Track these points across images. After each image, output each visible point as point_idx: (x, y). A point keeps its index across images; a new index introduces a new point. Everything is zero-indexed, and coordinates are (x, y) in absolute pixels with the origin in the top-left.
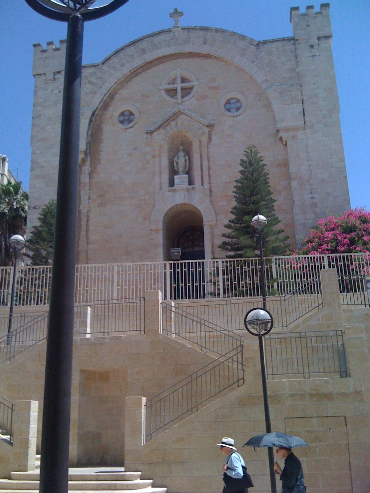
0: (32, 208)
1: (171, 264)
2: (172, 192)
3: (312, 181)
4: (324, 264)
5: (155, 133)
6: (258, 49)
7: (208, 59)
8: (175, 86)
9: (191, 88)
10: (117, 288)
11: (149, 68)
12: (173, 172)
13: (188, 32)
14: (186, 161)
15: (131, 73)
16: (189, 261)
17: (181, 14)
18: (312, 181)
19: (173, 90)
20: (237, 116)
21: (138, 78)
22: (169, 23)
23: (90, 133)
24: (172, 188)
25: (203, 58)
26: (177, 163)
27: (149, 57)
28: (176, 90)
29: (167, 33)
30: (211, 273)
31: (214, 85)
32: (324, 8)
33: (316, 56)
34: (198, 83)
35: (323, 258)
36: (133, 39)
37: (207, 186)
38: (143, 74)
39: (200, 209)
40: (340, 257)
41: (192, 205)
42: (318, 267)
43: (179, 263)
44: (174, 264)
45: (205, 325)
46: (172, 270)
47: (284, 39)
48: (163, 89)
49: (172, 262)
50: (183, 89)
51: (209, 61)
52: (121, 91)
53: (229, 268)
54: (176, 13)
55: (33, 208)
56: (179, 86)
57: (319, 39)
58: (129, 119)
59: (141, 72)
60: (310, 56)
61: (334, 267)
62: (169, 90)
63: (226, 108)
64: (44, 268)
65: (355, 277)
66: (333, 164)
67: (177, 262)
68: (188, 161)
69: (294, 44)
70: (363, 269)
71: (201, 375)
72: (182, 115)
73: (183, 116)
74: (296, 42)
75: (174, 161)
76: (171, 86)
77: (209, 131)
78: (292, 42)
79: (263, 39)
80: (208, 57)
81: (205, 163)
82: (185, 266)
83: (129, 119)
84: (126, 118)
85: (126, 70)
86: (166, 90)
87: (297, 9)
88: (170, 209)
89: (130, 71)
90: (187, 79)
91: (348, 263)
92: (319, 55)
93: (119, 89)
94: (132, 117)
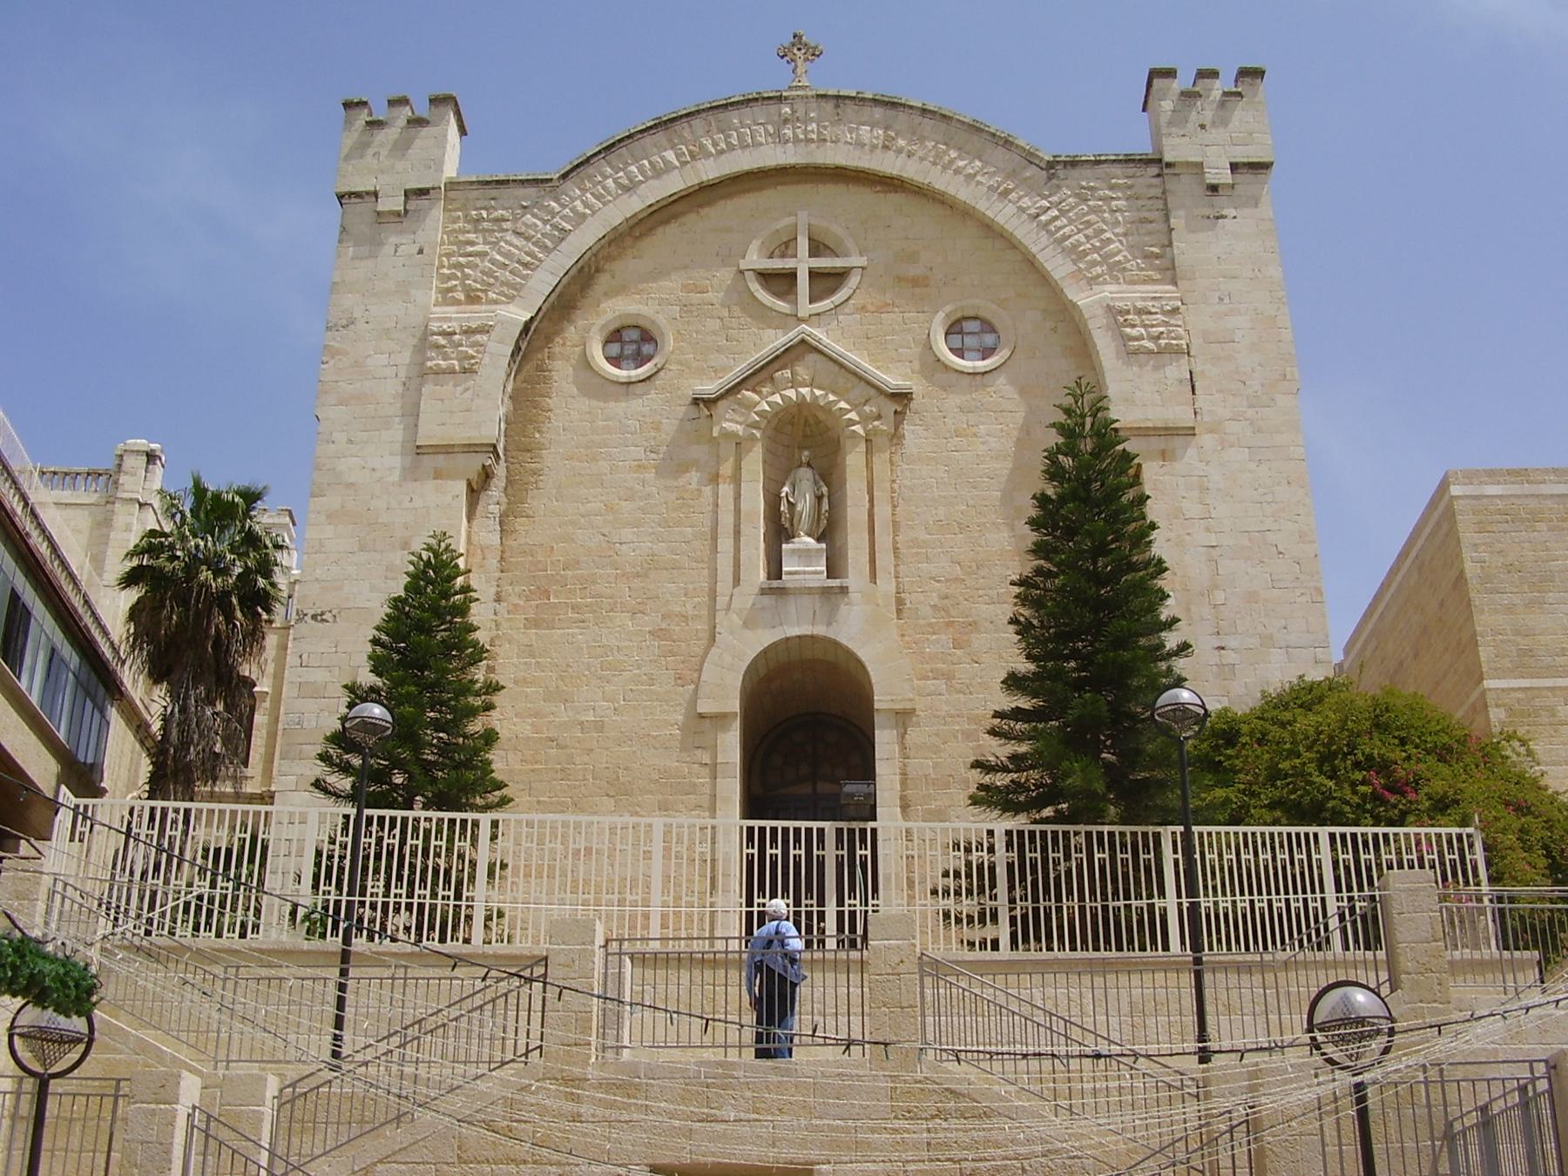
0: (308, 619)
1: (839, 831)
2: (774, 597)
3: (1220, 597)
4: (1176, 856)
5: (721, 404)
6: (1050, 179)
7: (896, 192)
8: (789, 264)
9: (839, 274)
10: (838, 912)
11: (709, 203)
12: (779, 531)
13: (837, 106)
14: (819, 498)
15: (651, 213)
16: (797, 824)
17: (814, 53)
18: (1220, 597)
19: (783, 274)
20: (986, 372)
21: (672, 230)
22: (774, 78)
23: (509, 389)
24: (775, 584)
25: (879, 188)
26: (791, 505)
27: (709, 170)
28: (791, 276)
29: (771, 102)
30: (960, 873)
31: (914, 271)
32: (1247, 80)
33: (1223, 217)
34: (862, 261)
35: (1316, 835)
36: (666, 112)
37: (886, 585)
38: (691, 217)
39: (862, 654)
40: (1449, 836)
41: (836, 644)
42: (1369, 869)
43: (866, 829)
44: (851, 831)
45: (1462, 1117)
46: (845, 853)
47: (1129, 160)
48: (753, 270)
49: (844, 825)
50: (814, 274)
51: (896, 198)
52: (617, 266)
53: (1061, 855)
54: (798, 48)
55: (314, 617)
56: (803, 263)
57: (1234, 167)
58: (638, 352)
59: (683, 214)
60: (1208, 218)
61: (1433, 867)
62: (770, 274)
63: (994, 335)
64: (441, 820)
65: (1134, 903)
66: (1281, 548)
67: (862, 825)
68: (825, 500)
69: (1159, 175)
70: (503, 873)
71: (305, 1094)
72: (811, 355)
73: (812, 358)
74: (1166, 171)
75: (780, 498)
76: (777, 264)
77: (896, 412)
78: (1154, 170)
79: (1065, 152)
80: (895, 186)
81: (883, 512)
82: (797, 840)
83: (638, 352)
84: (630, 349)
85: (635, 204)
86: (759, 273)
87: (1170, 73)
88: (765, 652)
89: (650, 206)
90: (827, 247)
91: (1471, 857)
92: (1235, 217)
93: (610, 258)
94: (647, 349)
